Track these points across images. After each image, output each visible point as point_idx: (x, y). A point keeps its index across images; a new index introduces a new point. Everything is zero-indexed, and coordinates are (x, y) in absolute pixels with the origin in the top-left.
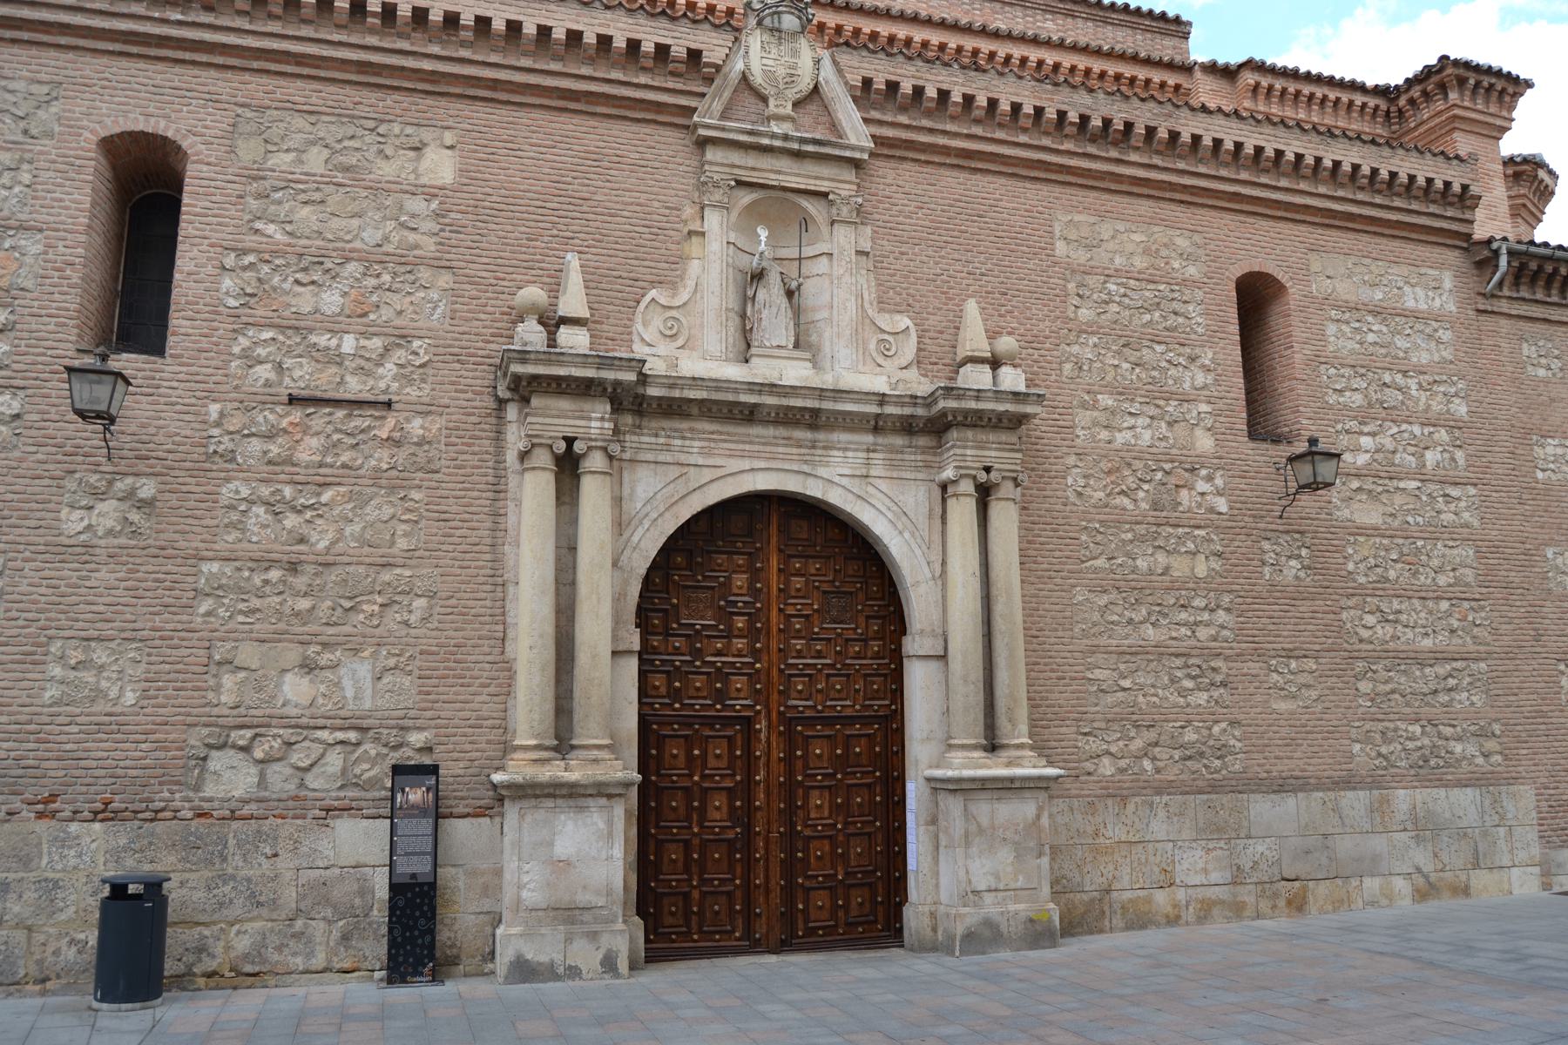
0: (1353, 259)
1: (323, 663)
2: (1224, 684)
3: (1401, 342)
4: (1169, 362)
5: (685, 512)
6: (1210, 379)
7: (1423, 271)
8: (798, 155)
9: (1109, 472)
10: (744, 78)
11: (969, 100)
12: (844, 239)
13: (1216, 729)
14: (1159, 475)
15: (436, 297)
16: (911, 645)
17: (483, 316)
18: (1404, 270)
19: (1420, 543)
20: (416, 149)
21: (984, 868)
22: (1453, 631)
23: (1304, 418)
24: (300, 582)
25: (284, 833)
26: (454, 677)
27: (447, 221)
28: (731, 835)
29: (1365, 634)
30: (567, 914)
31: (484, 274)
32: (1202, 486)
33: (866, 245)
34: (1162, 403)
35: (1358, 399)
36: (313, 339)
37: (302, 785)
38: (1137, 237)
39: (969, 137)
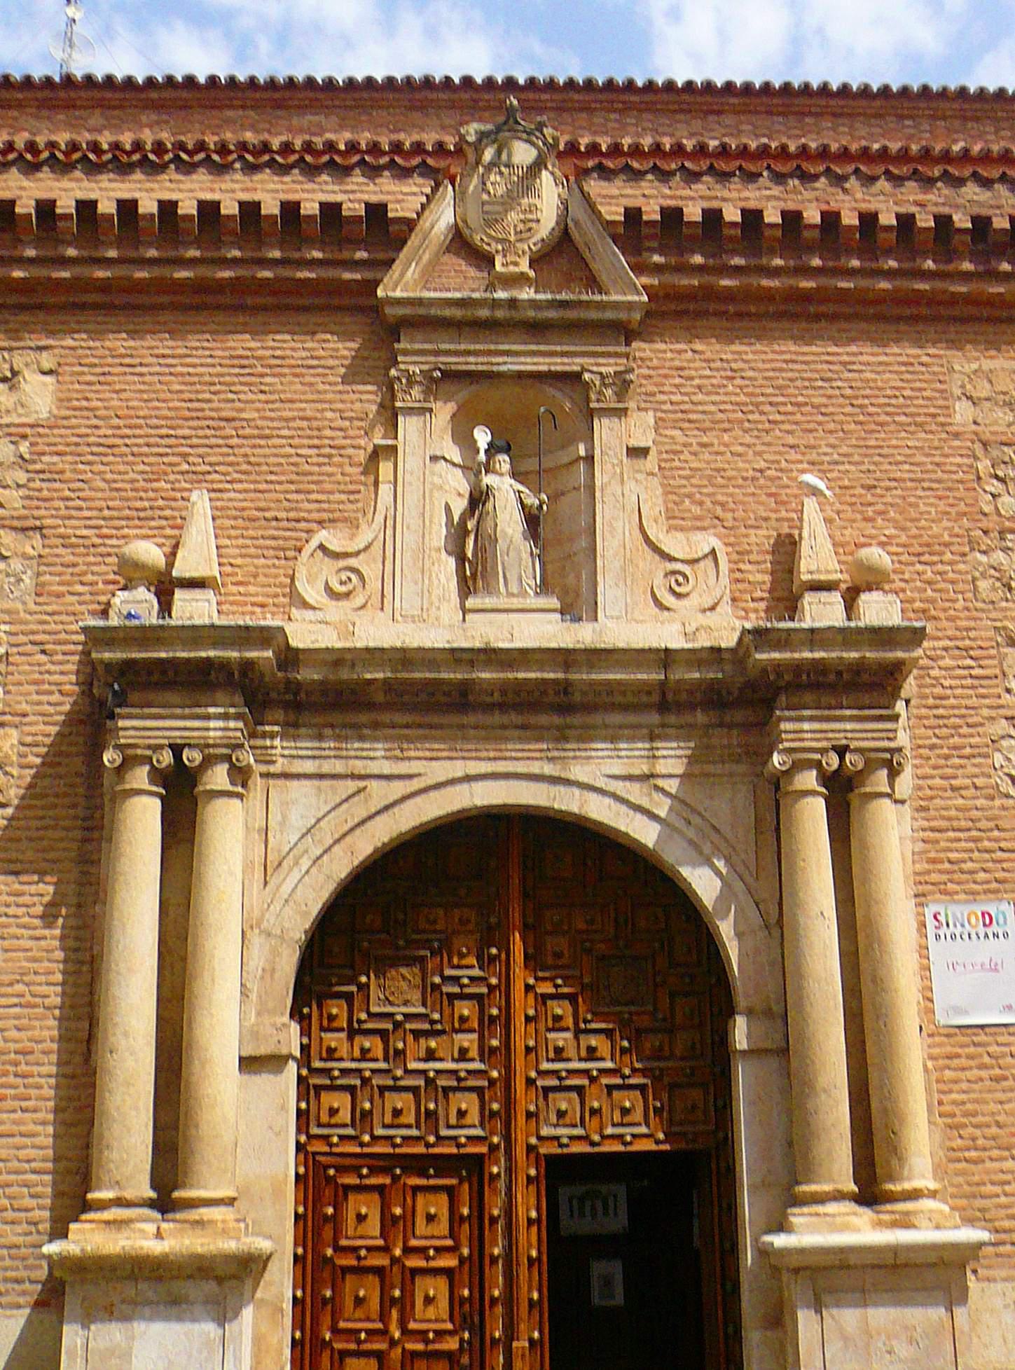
5: (365, 845)
15: (19, 567)
17: (79, 588)
26: (15, 1098)
27: (38, 467)
28: (452, 1344)
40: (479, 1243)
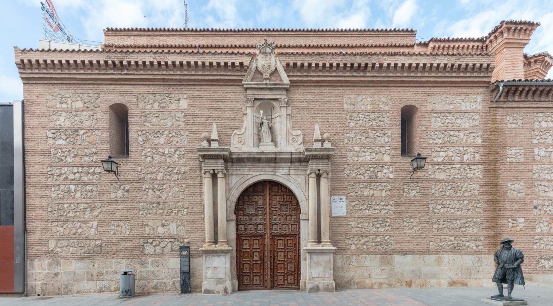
0: (443, 96)
2: (389, 226)
3: (459, 121)
5: (244, 186)
6: (390, 139)
7: (470, 97)
8: (271, 89)
9: (357, 169)
10: (257, 69)
11: (317, 65)
12: (283, 111)
13: (386, 238)
14: (372, 169)
16: (301, 217)
18: (463, 97)
19: (459, 184)
20: (179, 100)
21: (317, 271)
22: (468, 210)
23: (418, 148)
24: (160, 206)
25: (160, 261)
28: (259, 262)
29: (437, 211)
30: (220, 281)
32: (385, 171)
33: (289, 112)
35: (440, 141)
37: (163, 251)
38: (369, 100)
39: (318, 76)
40: (263, 248)
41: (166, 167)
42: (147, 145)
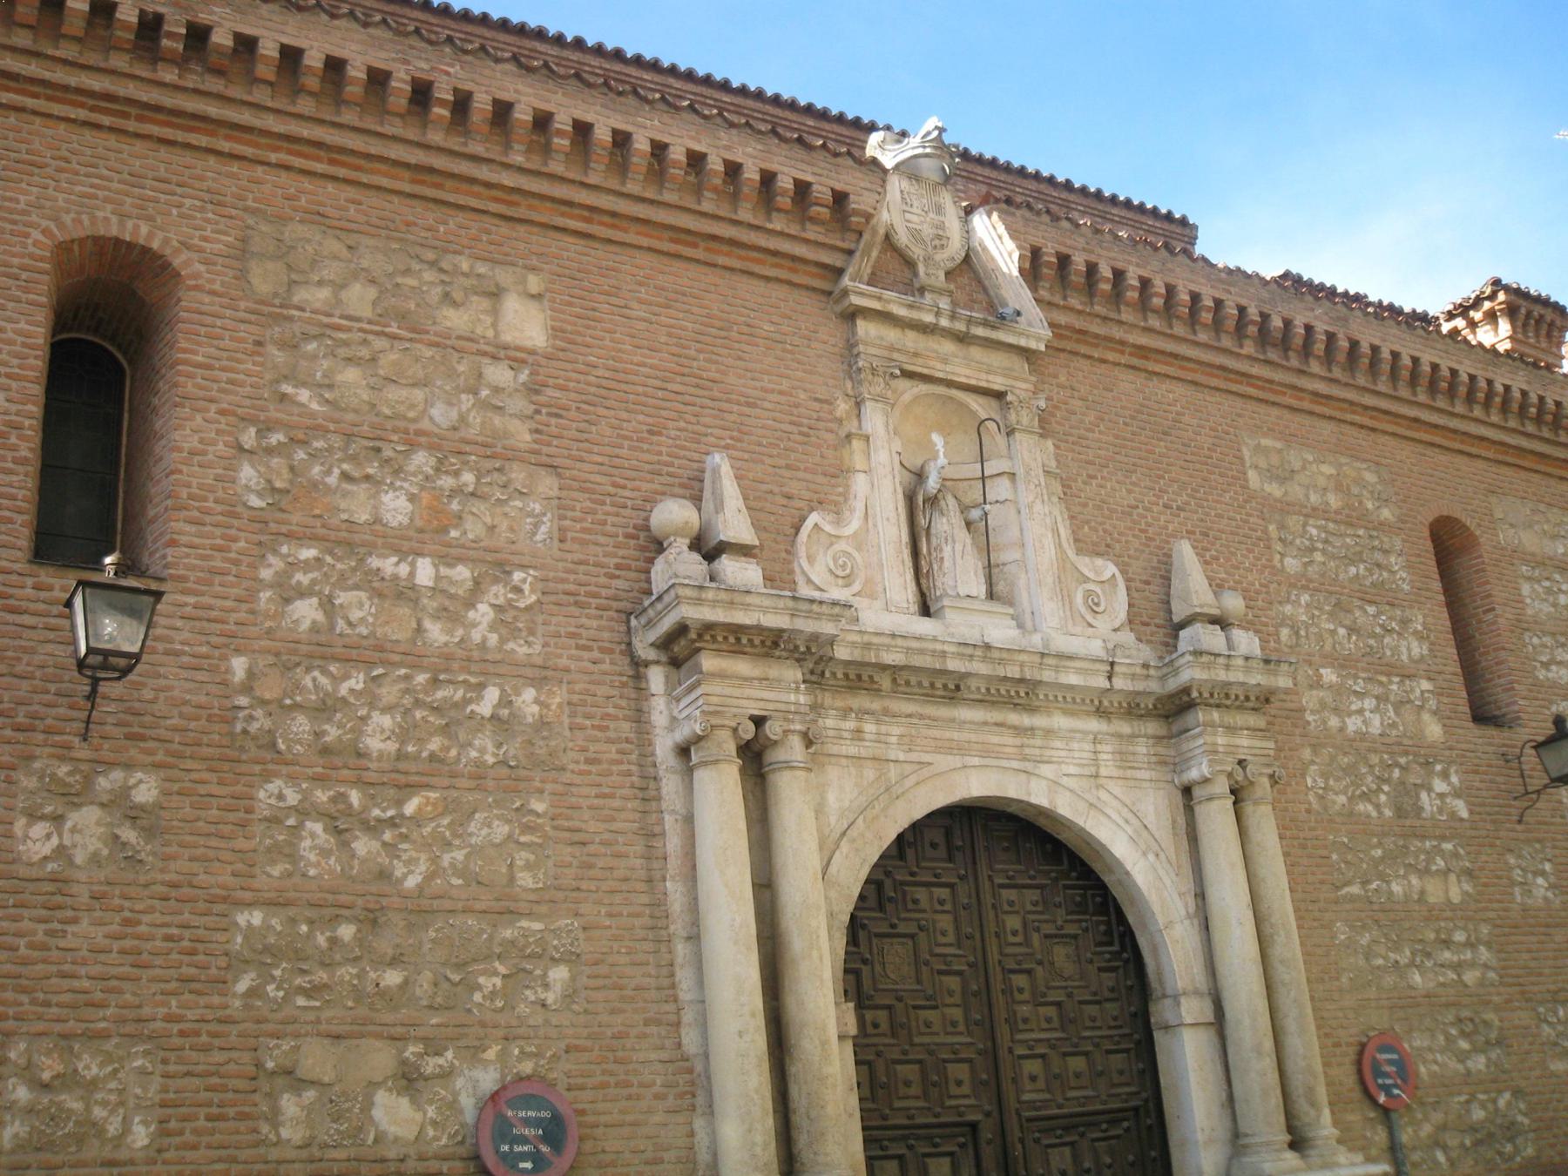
1: (429, 1070)
2: (1499, 1043)
4: (1382, 626)
14: (1396, 773)
15: (538, 508)
17: (602, 539)
31: (599, 478)
34: (1384, 679)
36: (374, 562)
38: (1327, 469)
41: (421, 678)
42: (296, 518)
